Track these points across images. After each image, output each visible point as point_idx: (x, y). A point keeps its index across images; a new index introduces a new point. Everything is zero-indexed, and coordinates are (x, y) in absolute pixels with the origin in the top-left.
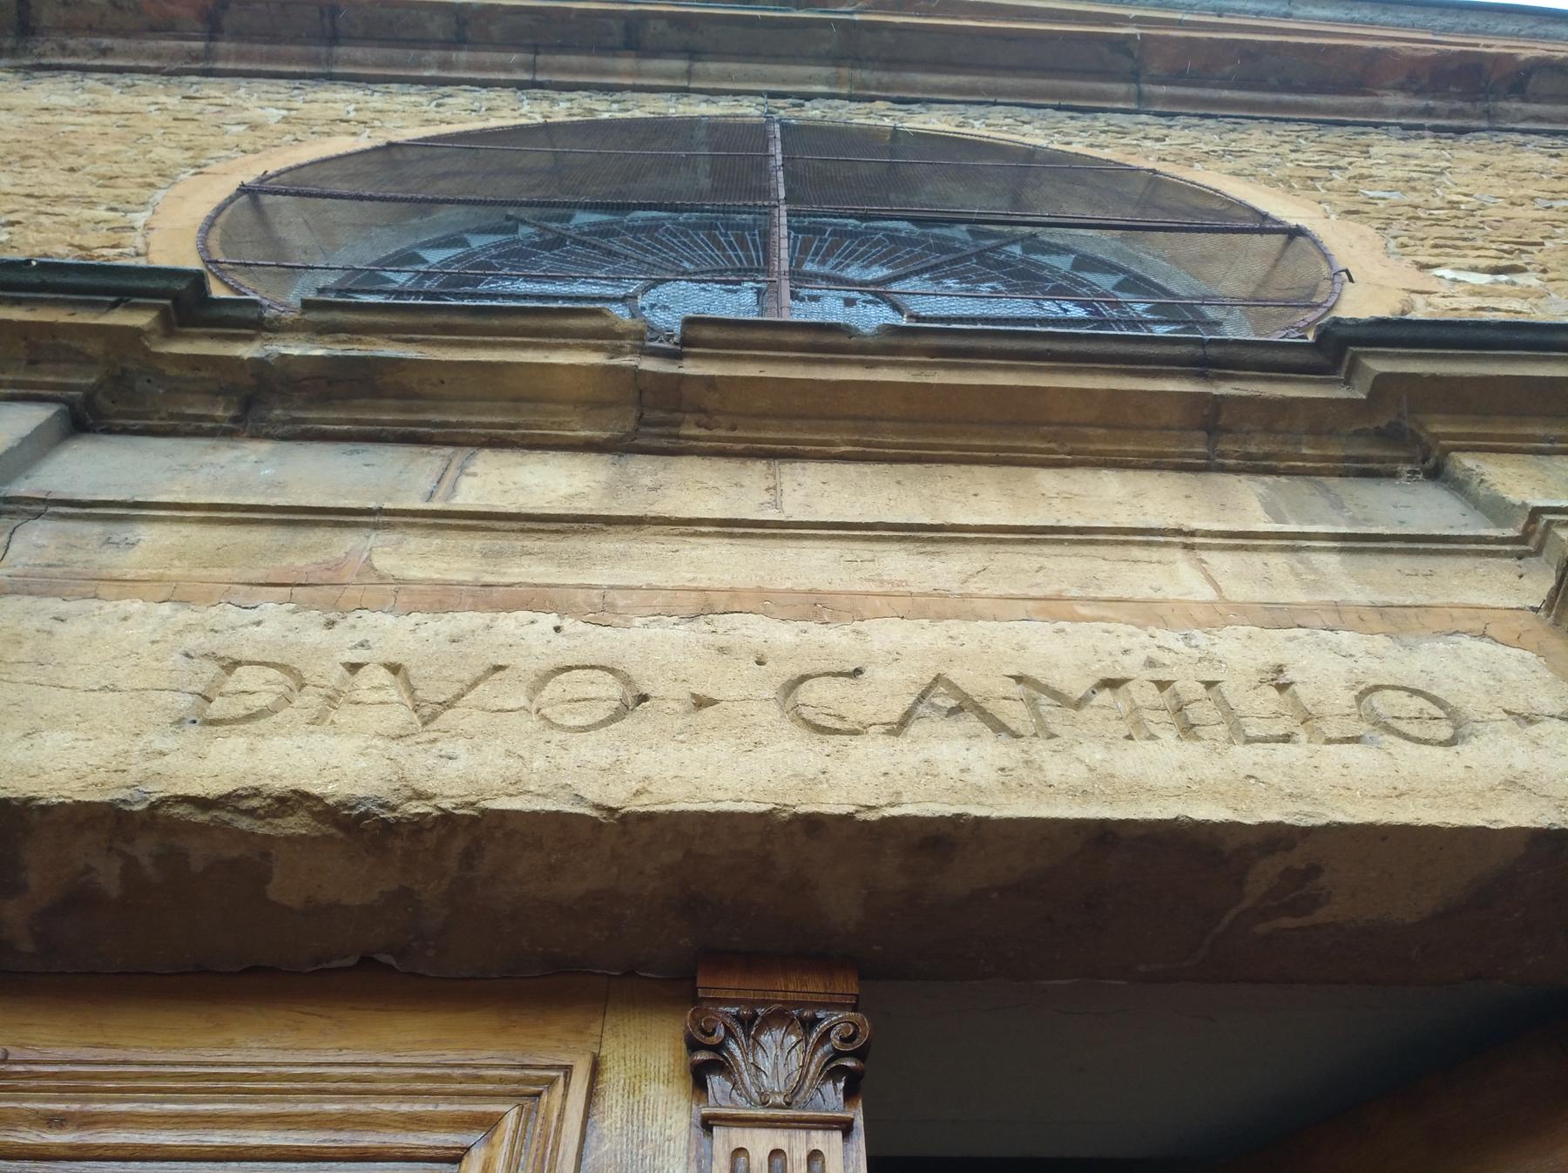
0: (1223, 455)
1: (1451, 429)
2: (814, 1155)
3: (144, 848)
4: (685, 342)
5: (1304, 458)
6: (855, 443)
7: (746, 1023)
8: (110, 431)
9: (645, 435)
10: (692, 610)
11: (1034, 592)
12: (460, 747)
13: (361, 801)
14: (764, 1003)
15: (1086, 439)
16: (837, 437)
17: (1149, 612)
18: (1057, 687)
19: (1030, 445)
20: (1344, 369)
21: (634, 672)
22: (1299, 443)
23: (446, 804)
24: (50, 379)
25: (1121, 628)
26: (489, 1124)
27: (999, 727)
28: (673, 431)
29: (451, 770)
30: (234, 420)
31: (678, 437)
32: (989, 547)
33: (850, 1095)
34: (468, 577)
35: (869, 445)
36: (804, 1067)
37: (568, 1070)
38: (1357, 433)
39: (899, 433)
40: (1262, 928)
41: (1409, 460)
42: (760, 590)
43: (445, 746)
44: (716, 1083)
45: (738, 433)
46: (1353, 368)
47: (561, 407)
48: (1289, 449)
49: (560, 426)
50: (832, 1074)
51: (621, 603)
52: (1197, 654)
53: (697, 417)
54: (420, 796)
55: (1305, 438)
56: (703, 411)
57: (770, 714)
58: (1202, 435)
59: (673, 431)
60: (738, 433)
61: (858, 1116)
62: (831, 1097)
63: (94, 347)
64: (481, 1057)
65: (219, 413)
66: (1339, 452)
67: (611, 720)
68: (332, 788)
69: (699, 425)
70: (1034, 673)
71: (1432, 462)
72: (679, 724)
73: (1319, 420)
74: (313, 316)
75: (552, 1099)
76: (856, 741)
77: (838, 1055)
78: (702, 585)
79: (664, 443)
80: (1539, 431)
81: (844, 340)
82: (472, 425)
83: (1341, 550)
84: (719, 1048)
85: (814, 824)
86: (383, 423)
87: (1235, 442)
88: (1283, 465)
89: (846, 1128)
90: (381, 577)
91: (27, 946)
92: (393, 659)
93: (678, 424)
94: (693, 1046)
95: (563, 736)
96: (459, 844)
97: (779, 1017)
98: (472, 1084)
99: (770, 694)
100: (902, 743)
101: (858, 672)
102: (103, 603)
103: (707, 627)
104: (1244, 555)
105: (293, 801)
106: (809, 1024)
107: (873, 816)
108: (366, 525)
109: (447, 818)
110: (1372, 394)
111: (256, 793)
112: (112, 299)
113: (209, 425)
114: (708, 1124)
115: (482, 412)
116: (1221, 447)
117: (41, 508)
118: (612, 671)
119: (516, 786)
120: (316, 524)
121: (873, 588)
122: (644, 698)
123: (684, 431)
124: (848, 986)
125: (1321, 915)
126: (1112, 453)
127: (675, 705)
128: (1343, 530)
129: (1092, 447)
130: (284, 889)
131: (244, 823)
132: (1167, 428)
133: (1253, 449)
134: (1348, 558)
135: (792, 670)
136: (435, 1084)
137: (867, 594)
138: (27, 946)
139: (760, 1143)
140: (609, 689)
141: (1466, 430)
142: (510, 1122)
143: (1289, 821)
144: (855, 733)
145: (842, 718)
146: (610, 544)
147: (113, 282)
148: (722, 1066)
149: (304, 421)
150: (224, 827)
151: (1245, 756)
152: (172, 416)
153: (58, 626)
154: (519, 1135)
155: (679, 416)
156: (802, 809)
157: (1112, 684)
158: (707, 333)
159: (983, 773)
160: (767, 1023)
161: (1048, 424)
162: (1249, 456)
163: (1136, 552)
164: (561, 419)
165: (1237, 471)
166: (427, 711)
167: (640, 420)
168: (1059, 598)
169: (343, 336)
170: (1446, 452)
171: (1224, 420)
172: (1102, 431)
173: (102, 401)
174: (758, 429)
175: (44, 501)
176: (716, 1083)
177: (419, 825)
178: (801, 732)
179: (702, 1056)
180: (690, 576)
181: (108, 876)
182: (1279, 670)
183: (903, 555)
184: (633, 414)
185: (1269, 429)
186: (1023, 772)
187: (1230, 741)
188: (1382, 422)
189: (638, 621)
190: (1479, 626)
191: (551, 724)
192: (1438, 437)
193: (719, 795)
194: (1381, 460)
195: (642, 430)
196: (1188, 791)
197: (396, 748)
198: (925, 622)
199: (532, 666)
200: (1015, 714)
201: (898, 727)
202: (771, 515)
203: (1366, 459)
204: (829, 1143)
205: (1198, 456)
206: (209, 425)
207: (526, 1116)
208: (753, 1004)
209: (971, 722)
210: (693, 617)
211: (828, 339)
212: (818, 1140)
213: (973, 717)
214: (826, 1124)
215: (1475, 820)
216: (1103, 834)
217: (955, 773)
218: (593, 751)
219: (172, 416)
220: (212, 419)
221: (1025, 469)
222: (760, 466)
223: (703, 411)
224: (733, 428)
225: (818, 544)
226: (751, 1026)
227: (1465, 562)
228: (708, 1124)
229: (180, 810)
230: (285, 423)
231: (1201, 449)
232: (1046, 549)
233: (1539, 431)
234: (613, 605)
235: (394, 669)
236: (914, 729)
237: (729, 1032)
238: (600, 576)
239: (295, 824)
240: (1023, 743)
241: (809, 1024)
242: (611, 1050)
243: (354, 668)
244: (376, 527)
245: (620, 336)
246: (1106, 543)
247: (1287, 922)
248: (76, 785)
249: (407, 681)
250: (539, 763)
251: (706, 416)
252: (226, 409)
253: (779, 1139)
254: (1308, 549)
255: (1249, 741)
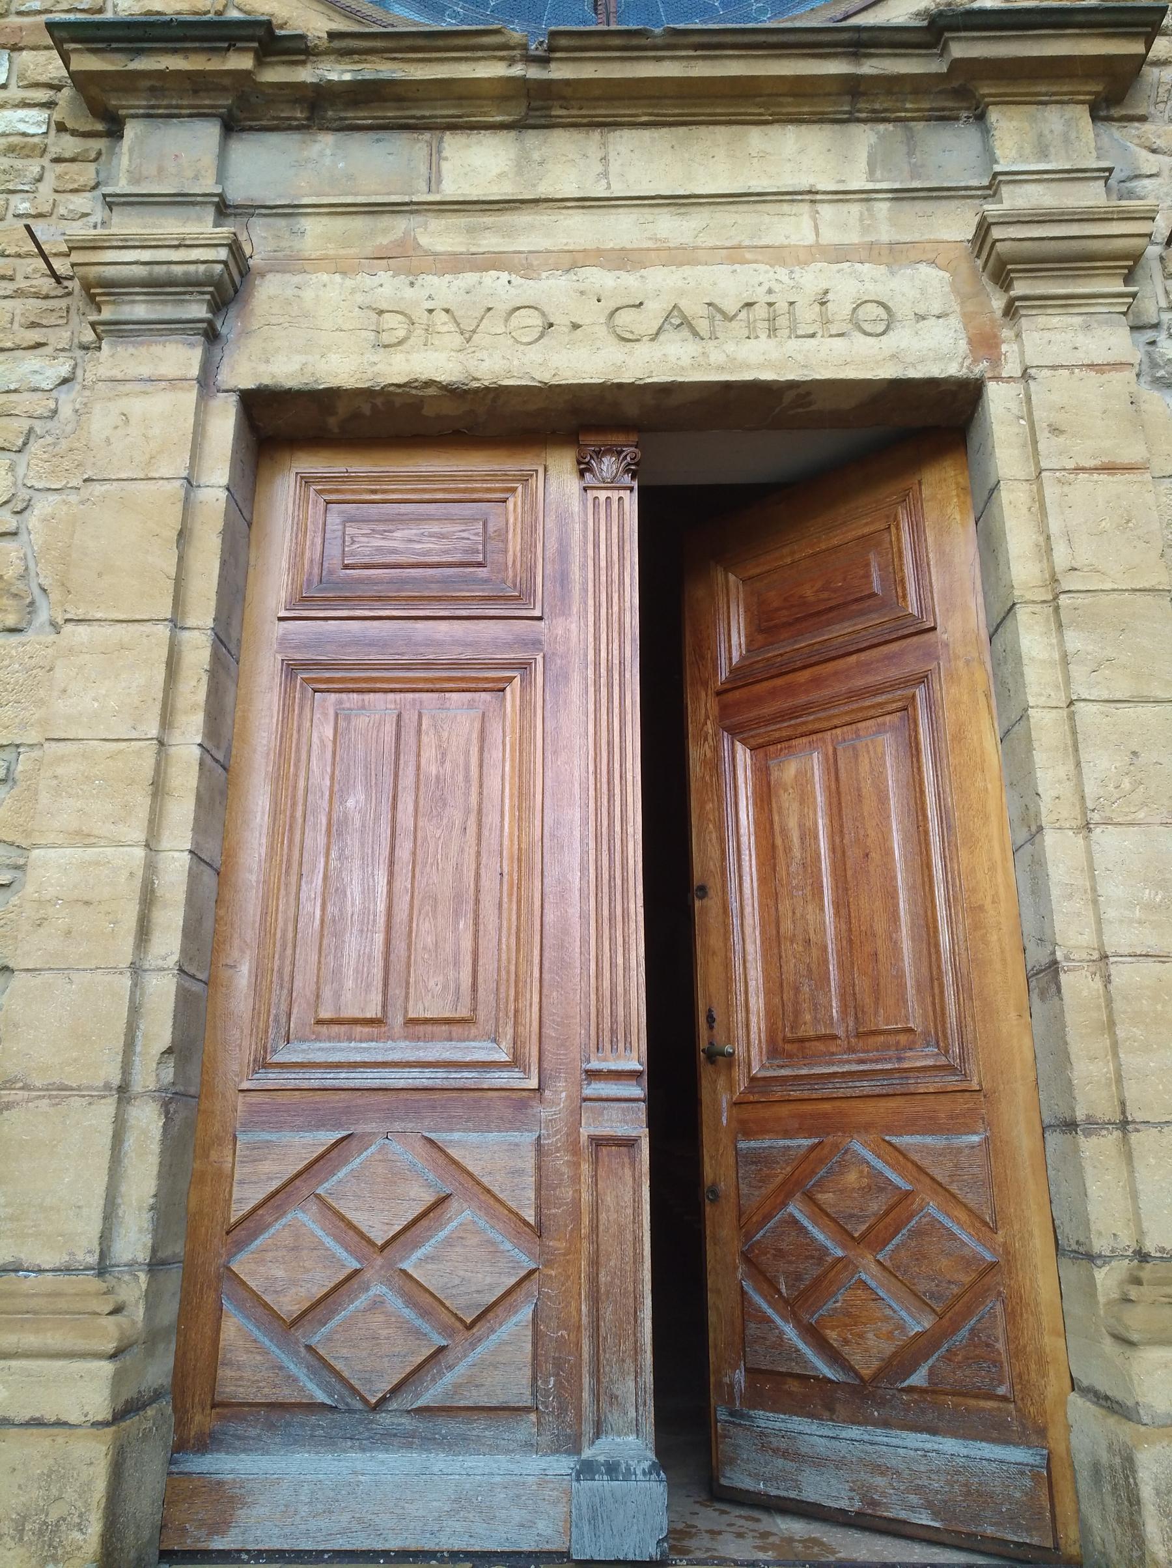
0: (859, 111)
1: (993, 91)
2: (620, 498)
3: (379, 401)
4: (551, 49)
5: (906, 110)
6: (651, 115)
7: (598, 453)
8: (243, 130)
9: (532, 117)
10: (567, 267)
11: (728, 244)
12: (484, 354)
13: (455, 383)
14: (604, 445)
15: (781, 105)
16: (640, 111)
17: (778, 255)
18: (724, 309)
19: (749, 111)
20: (940, 46)
21: (546, 309)
22: (904, 101)
23: (486, 383)
24: (207, 102)
25: (762, 267)
26: (514, 490)
27: (696, 334)
28: (547, 112)
29: (485, 366)
30: (308, 119)
31: (551, 117)
32: (712, 208)
33: (633, 478)
34: (463, 249)
35: (657, 115)
36: (618, 469)
37: (536, 471)
38: (940, 92)
39: (676, 106)
40: (791, 412)
41: (968, 109)
42: (598, 250)
43: (479, 355)
44: (587, 475)
45: (584, 112)
46: (945, 48)
47: (485, 102)
48: (899, 104)
49: (485, 114)
50: (627, 471)
51: (535, 263)
52: (792, 283)
53: (560, 102)
54: (475, 379)
55: (909, 97)
56: (564, 98)
57: (602, 331)
58: (848, 98)
59: (547, 112)
60: (584, 112)
61: (635, 484)
62: (627, 479)
63: (227, 81)
64: (506, 467)
65: (299, 115)
66: (928, 106)
67: (541, 337)
68: (443, 377)
69: (561, 107)
70: (716, 301)
71: (980, 110)
72: (567, 339)
73: (916, 85)
74: (337, 44)
75: (532, 481)
76: (637, 345)
77: (629, 464)
78: (571, 248)
79: (543, 121)
80: (1043, 89)
81: (643, 42)
82: (436, 117)
83: (892, 199)
84: (588, 463)
85: (620, 386)
86: (389, 118)
87: (868, 101)
88: (893, 116)
89: (631, 489)
90: (426, 251)
91: (336, 430)
92: (446, 306)
93: (549, 108)
94: (579, 463)
95: (523, 347)
96: (491, 396)
97: (609, 451)
98: (505, 477)
99: (603, 320)
100: (655, 345)
101: (641, 304)
102: (309, 276)
103: (575, 278)
104: (840, 205)
105: (430, 383)
106: (619, 453)
107: (642, 382)
108: (406, 212)
109: (487, 388)
110: (950, 69)
111: (416, 380)
112: (226, 45)
113: (295, 123)
114: (585, 489)
115: (442, 108)
116: (859, 106)
117: (252, 211)
118: (536, 309)
119: (509, 374)
120: (383, 212)
121: (650, 244)
122: (551, 325)
123: (553, 113)
124: (634, 438)
125: (813, 408)
126: (794, 114)
127: (564, 328)
128: (897, 186)
129: (784, 110)
130: (427, 411)
131: (414, 392)
132: (829, 94)
133: (877, 106)
134: (894, 203)
135: (613, 305)
136: (493, 477)
137: (648, 250)
138: (336, 430)
139: (602, 495)
140: (536, 320)
141: (1001, 90)
142: (520, 490)
143: (797, 379)
144: (638, 340)
145: (632, 332)
146: (522, 219)
147: (225, 32)
148: (590, 469)
149: (346, 119)
150: (408, 394)
151: (793, 345)
152: (274, 118)
153: (300, 292)
154: (524, 494)
155: (550, 103)
156: (615, 381)
157: (749, 305)
158: (563, 42)
159: (686, 361)
160: (605, 453)
161: (761, 96)
162: (874, 111)
163: (786, 207)
164: (485, 109)
165: (865, 121)
166: (467, 336)
167: (529, 108)
168: (739, 247)
169: (356, 57)
170: (988, 105)
171: (862, 89)
172: (790, 100)
173: (236, 112)
174: (594, 108)
175: (252, 206)
176: (587, 475)
177: (476, 391)
178: (616, 341)
179: (582, 466)
180: (565, 241)
181: (366, 409)
182: (826, 292)
183: (668, 217)
184: (524, 103)
185: (889, 93)
186: (700, 359)
187: (790, 337)
188: (955, 84)
189: (544, 275)
190: (932, 256)
191: (518, 342)
192: (984, 96)
193: (584, 375)
194: (951, 109)
195: (531, 113)
196: (767, 364)
197: (461, 356)
198: (674, 268)
199: (502, 307)
200: (703, 326)
201: (654, 338)
202: (600, 191)
203: (943, 109)
204: (625, 494)
205: (845, 113)
206: (295, 123)
207: (525, 487)
208: (600, 446)
209: (685, 332)
210: (568, 271)
211: (635, 41)
212: (622, 493)
213: (687, 330)
214: (625, 488)
215: (869, 376)
216: (727, 386)
217: (674, 360)
218: (534, 355)
219: (274, 118)
220: (296, 119)
221: (746, 127)
222: (596, 135)
223: (564, 98)
224: (581, 108)
225: (626, 210)
226: (599, 454)
227: (954, 204)
228: (585, 489)
229: (391, 389)
230: (336, 120)
231: (846, 108)
232: (741, 208)
233: (1043, 89)
234: (532, 265)
235: (447, 311)
236: (662, 338)
237: (592, 457)
238: (524, 243)
239: (431, 391)
240: (704, 343)
241: (619, 453)
242: (550, 462)
243: (430, 311)
244: (411, 212)
245: (513, 48)
246: (771, 201)
247: (800, 410)
248: (352, 380)
249: (454, 318)
250: (516, 362)
251: (566, 104)
252: (302, 112)
253: (609, 493)
254: (875, 199)
255: (798, 337)
